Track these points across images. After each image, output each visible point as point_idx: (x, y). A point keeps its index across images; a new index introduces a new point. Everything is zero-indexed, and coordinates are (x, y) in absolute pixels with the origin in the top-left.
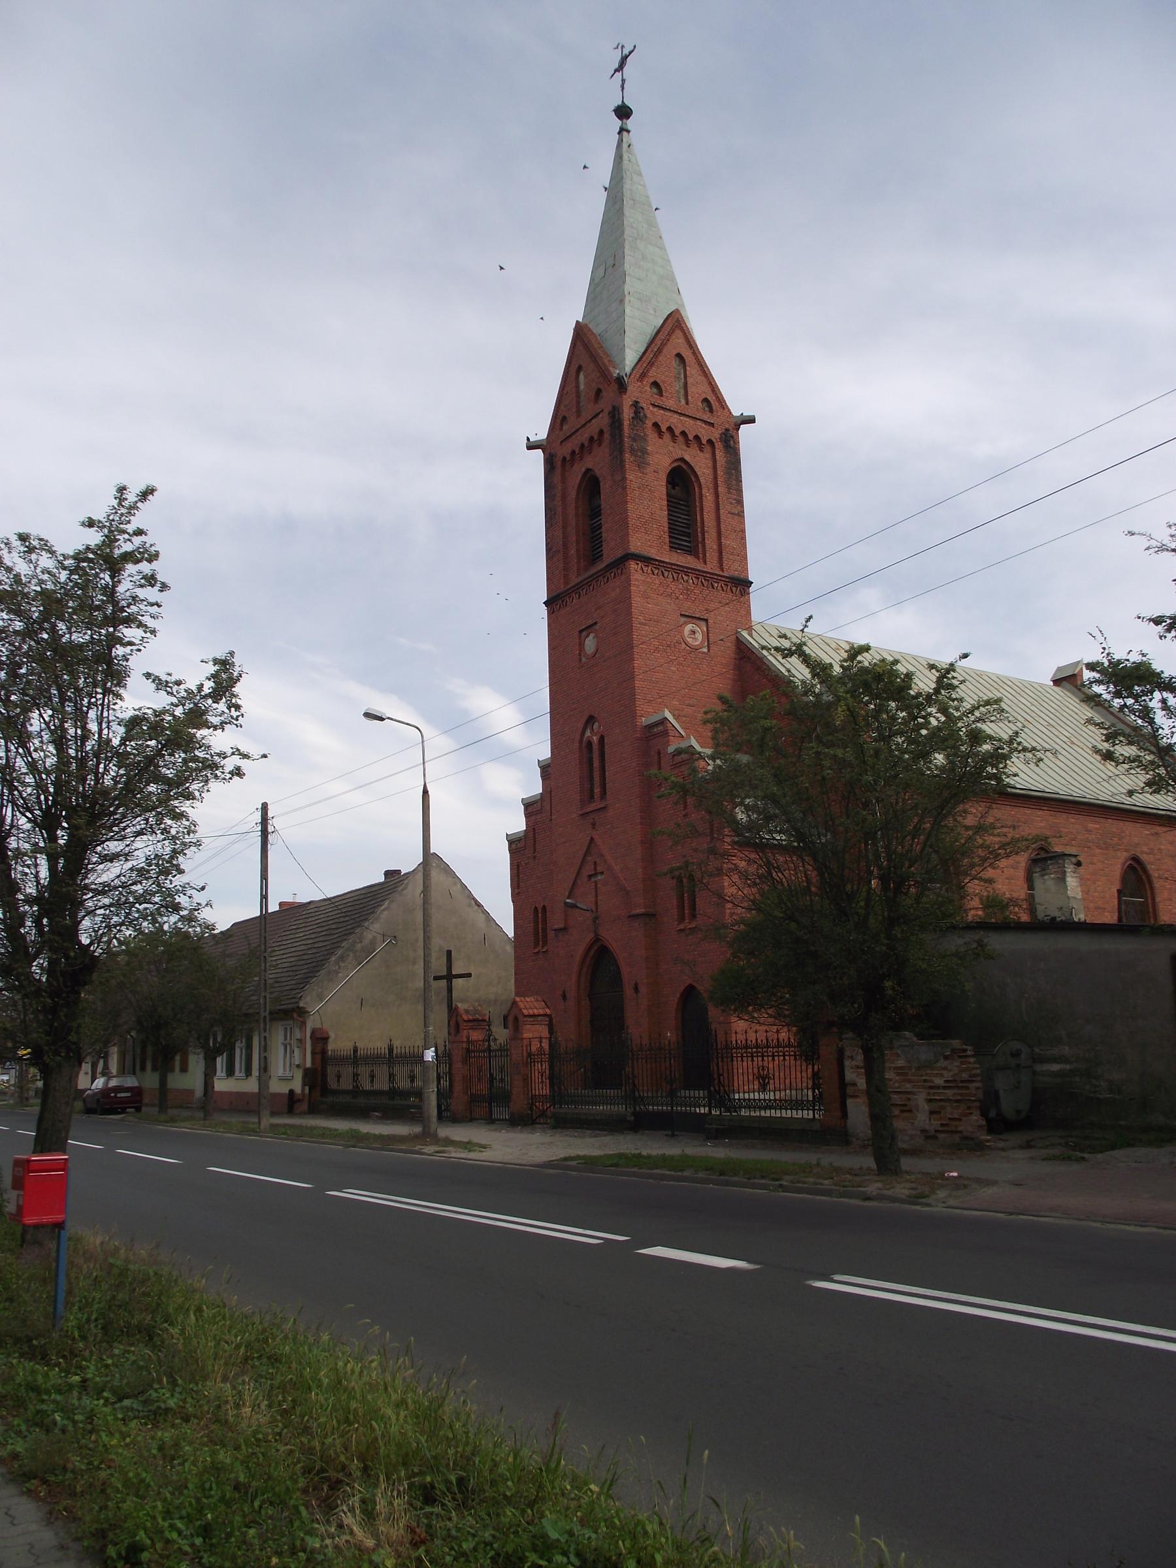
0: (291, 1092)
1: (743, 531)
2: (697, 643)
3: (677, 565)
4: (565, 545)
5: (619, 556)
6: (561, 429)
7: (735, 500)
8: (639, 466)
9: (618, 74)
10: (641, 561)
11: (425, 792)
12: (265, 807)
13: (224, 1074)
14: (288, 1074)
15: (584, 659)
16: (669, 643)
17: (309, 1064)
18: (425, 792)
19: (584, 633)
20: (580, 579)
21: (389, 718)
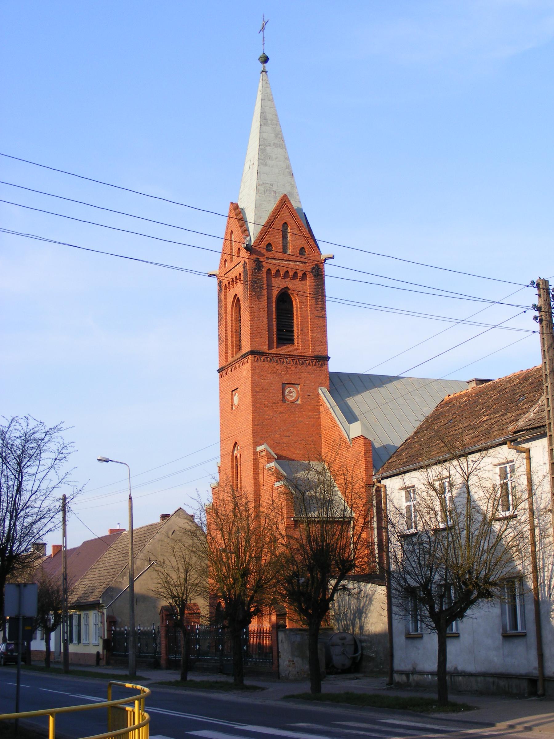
0: (98, 653)
1: (325, 326)
2: (294, 398)
3: (281, 354)
4: (226, 337)
5: (247, 351)
6: (225, 267)
7: (320, 308)
8: (258, 298)
9: (266, 20)
10: (257, 355)
11: (130, 499)
12: (99, 460)
13: (76, 642)
14: (97, 642)
15: (234, 408)
16: (274, 401)
17: (106, 637)
18: (130, 499)
19: (234, 392)
20: (233, 359)
21: (110, 461)
